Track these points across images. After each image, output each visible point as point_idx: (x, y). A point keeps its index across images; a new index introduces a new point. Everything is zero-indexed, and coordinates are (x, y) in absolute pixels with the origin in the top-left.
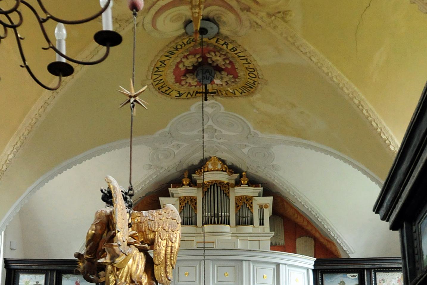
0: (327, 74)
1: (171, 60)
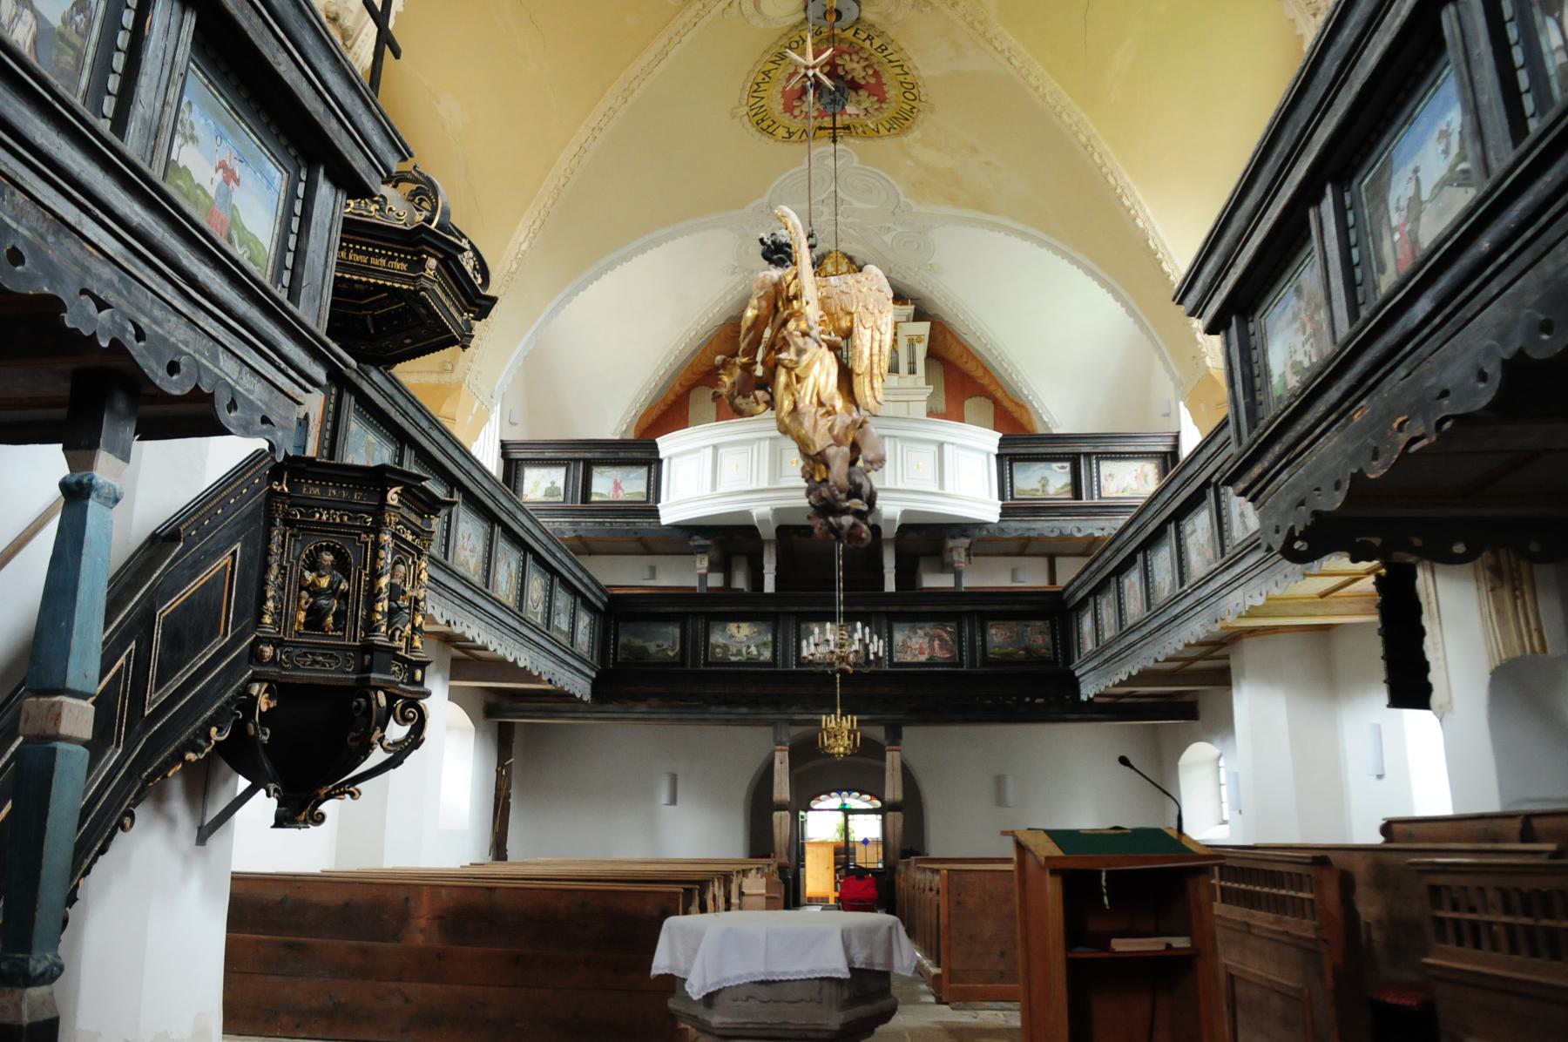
0: (1037, 89)
1: (780, 71)
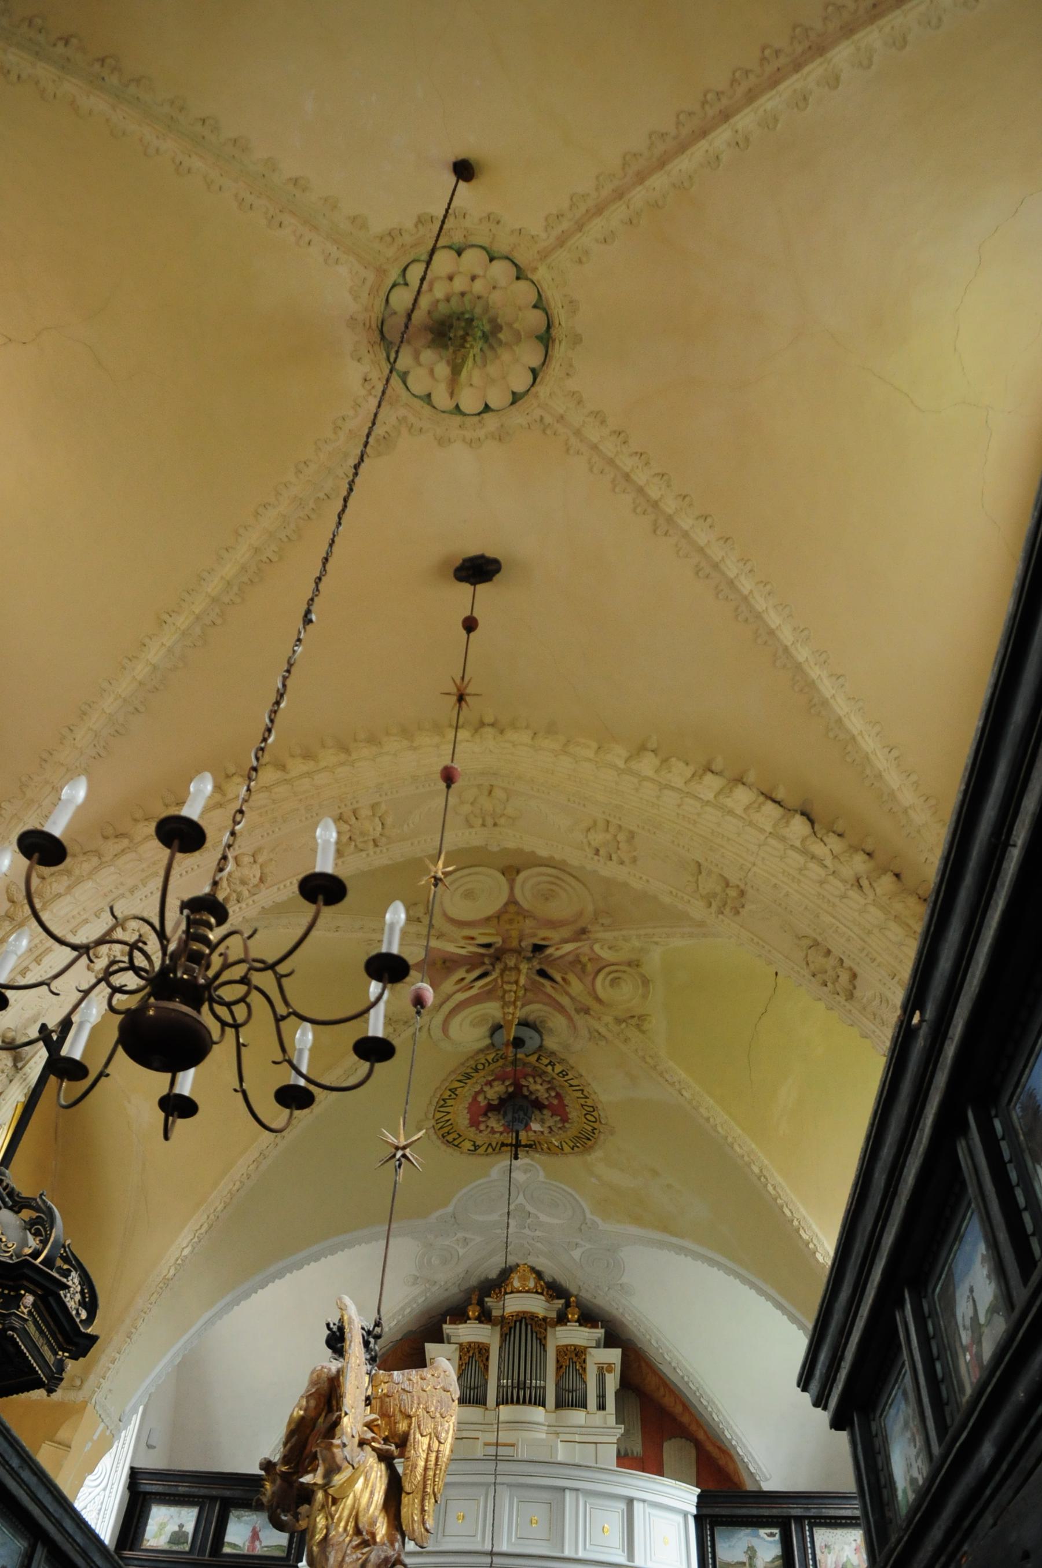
0: (708, 1119)
1: (466, 1088)
